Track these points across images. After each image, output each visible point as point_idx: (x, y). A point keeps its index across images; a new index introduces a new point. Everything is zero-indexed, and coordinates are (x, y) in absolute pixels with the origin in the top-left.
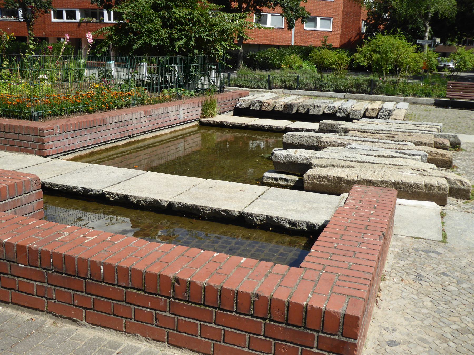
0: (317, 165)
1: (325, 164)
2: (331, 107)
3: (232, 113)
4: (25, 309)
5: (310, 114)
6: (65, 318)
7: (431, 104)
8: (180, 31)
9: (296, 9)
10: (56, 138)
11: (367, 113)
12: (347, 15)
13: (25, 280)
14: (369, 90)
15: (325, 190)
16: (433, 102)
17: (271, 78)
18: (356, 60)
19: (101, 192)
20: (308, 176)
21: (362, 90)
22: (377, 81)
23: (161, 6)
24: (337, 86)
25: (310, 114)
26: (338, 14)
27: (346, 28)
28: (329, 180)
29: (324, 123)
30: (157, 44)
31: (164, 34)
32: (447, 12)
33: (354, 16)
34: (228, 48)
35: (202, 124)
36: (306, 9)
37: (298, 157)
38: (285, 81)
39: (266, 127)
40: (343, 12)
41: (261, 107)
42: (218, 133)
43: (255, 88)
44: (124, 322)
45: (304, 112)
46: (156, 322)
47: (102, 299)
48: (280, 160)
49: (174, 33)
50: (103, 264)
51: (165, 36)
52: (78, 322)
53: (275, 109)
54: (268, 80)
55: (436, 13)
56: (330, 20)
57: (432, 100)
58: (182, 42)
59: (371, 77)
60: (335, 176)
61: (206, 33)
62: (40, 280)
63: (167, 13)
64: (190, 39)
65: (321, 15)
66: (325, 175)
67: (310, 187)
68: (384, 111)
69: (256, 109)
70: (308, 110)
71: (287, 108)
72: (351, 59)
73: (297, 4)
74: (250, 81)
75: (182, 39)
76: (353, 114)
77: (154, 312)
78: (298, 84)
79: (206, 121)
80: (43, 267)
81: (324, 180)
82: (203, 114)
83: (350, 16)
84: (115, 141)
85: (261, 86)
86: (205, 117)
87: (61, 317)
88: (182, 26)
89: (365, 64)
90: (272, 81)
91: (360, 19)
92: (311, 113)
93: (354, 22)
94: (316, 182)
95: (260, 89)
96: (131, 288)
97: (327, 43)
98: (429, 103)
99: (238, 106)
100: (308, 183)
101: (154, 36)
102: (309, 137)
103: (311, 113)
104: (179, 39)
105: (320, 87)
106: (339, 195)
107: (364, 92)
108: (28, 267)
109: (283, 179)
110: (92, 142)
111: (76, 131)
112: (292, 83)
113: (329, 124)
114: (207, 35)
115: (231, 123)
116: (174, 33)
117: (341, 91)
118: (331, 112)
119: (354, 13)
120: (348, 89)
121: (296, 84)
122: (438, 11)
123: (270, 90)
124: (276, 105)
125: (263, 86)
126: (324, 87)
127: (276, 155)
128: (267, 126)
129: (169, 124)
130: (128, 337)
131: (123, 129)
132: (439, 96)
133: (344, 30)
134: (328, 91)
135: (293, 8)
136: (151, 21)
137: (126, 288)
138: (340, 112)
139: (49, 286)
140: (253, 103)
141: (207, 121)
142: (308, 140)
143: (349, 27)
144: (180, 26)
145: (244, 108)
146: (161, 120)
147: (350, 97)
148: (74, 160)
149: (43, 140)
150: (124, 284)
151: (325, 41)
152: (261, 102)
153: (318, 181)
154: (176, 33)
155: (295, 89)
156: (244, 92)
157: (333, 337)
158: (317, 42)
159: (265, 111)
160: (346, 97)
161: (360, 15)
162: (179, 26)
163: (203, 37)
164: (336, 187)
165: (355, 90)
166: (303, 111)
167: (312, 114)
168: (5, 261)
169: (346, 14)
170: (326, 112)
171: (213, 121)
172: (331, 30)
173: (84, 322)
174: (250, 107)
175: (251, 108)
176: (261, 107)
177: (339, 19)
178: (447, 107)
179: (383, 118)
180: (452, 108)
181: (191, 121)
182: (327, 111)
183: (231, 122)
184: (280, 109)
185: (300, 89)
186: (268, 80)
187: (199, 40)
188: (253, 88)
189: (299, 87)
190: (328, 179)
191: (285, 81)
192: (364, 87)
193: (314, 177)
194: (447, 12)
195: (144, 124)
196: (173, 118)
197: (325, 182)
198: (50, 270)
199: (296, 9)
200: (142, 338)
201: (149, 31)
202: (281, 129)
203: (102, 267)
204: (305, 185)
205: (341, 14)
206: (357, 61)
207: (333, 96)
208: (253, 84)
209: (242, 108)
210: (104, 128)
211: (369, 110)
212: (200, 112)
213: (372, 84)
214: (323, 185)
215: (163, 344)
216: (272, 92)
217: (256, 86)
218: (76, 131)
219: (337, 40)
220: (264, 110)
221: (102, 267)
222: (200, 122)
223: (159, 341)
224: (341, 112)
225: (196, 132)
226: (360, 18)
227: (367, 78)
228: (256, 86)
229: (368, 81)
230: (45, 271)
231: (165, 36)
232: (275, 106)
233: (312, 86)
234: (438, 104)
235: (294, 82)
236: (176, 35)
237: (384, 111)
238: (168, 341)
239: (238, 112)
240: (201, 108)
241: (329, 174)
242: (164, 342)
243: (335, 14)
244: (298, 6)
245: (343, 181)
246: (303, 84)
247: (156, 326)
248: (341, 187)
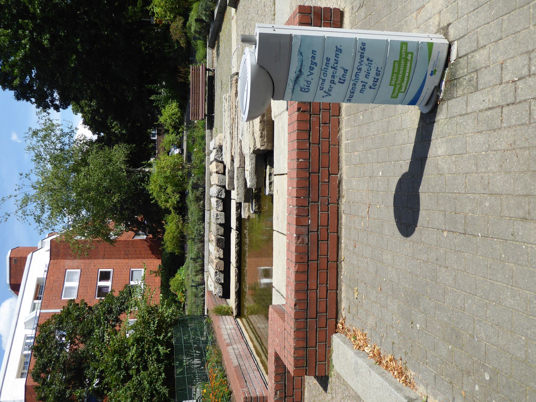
0: (254, 146)
1: (253, 140)
2: (217, 205)
3: (227, 300)
4: (340, 222)
5: (224, 222)
6: (339, 191)
7: (212, 132)
8: (149, 353)
9: (122, 299)
10: (253, 391)
11: (220, 172)
12: (127, 255)
13: (319, 220)
14: (201, 189)
15: (271, 133)
16: (209, 130)
17: (193, 284)
18: (174, 204)
19: (254, 156)
20: (262, 146)
21: (201, 195)
22: (193, 182)
23: (125, 374)
24: (199, 219)
25: (224, 222)
26: (127, 263)
27: (141, 254)
28: (263, 130)
29: (228, 185)
30: (163, 372)
31: (154, 366)
32: (126, 152)
33: (129, 247)
34: (165, 306)
35: (239, 315)
36: (121, 290)
37: (250, 167)
38: (197, 272)
39: (237, 249)
40: (124, 258)
41: (220, 271)
42: (246, 297)
43: (204, 300)
44: (332, 146)
45: (223, 229)
46: (327, 124)
47: (320, 161)
48: (254, 181)
49: (152, 359)
50: (298, 159)
51: (155, 365)
52: (339, 180)
53: (222, 257)
54: (196, 287)
55: (125, 162)
56: (132, 271)
57: (207, 132)
58: (160, 348)
59: (189, 188)
60: (259, 125)
61: (152, 325)
62: (317, 208)
63: (133, 367)
64: (158, 341)
65: (128, 280)
66: (260, 133)
67: (270, 144)
68: (218, 156)
69: (223, 277)
70: (220, 225)
71: (220, 243)
72: (173, 209)
73: (116, 298)
74: (198, 306)
75: (158, 349)
76: (222, 182)
77: (321, 125)
78: (198, 257)
79: (235, 310)
80: (307, 204)
81: (263, 133)
82: (229, 315)
83: (129, 251)
84: (255, 361)
85: (202, 294)
86: (232, 313)
87: (339, 193)
88: (145, 352)
89: (178, 196)
90: (197, 283)
91: (132, 241)
92: (223, 221)
93: (134, 247)
94: (265, 140)
95: (205, 294)
96: (309, 140)
97: (156, 270)
98: (210, 134)
99: (221, 294)
100: (267, 146)
101: (155, 377)
102: (238, 180)
103: (223, 221)
104: (157, 351)
105: (200, 235)
106: (273, 121)
107: (203, 193)
108: (310, 217)
109: (269, 177)
110: (257, 373)
111: (246, 381)
112: (197, 265)
113: (229, 181)
114: (154, 324)
115: (236, 284)
116: (152, 359)
117: (204, 215)
118: (221, 204)
119: (126, 247)
120: (201, 209)
121: (199, 260)
122: (124, 161)
123: (206, 283)
124: (217, 256)
125: (202, 291)
126: (200, 232)
127: (250, 185)
128: (236, 248)
129: (239, 334)
130: (341, 144)
131: (244, 357)
132: (204, 128)
133: (143, 256)
134: (204, 228)
135: (122, 302)
136: (140, 383)
137: (310, 144)
138: (221, 195)
139: (320, 201)
140: (218, 281)
141: (235, 308)
142: (240, 180)
143: (140, 251)
144: (145, 353)
145: (223, 288)
146: (236, 338)
147: (208, 206)
148: (268, 354)
149: (255, 397)
150: (308, 145)
151: (155, 272)
152: (216, 272)
153: (264, 138)
154: (152, 357)
155: (203, 261)
156: (208, 295)
157: (312, 19)
158: (156, 283)
159: (224, 267)
160: (208, 209)
161: (128, 241)
162: (145, 355)
163: (156, 328)
164: (267, 124)
165: (202, 201)
166: (222, 231)
167: (224, 221)
168: (309, 236)
169: (127, 256)
170: (222, 209)
171: (236, 302)
172: (143, 270)
173: (339, 175)
174: (221, 284)
175: (223, 282)
176: (220, 271)
177: (131, 262)
178: (213, 117)
179: (223, 156)
180: (214, 113)
181: (238, 324)
182: (221, 208)
183: (235, 283)
184: (221, 252)
185: (203, 256)
186: (196, 287)
187: (158, 332)
188: (204, 302)
189: (201, 257)
190: (262, 130)
191: (197, 272)
192: (198, 193)
193: (262, 141)
194: (126, 152)
195: (240, 347)
196: (233, 331)
197: (265, 133)
198: (309, 200)
199: (122, 299)
200: (340, 133)
201: (151, 383)
202: (238, 234)
203: (300, 160)
204: (269, 148)
205: (127, 261)
206: (175, 203)
207: (209, 221)
208: (199, 302)
209: (223, 290)
210: (243, 367)
211: (218, 170)
212: (227, 317)
213: (195, 187)
214: (267, 134)
215: (340, 120)
216: (207, 280)
217: (202, 299)
218: (246, 381)
219: (153, 263)
220: (223, 268)
221: (300, 160)
222: (237, 317)
223: (339, 123)
224: (220, 193)
225: (249, 323)
226: (130, 241)
227: (190, 192)
228: (202, 299)
229: (193, 190)
230: (310, 204)
231: (155, 365)
232: (219, 258)
233: (200, 245)
234: (211, 126)
235: (197, 262)
236: (153, 357)
237: (218, 156)
238: (338, 116)
239: (226, 295)
240: (224, 317)
241: (258, 130)
242: (339, 119)
243: (127, 267)
244: (119, 298)
245: (263, 119)
246: (199, 253)
247: (330, 124)
248: (267, 120)
